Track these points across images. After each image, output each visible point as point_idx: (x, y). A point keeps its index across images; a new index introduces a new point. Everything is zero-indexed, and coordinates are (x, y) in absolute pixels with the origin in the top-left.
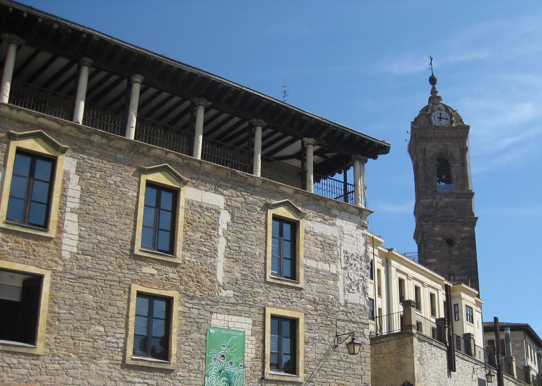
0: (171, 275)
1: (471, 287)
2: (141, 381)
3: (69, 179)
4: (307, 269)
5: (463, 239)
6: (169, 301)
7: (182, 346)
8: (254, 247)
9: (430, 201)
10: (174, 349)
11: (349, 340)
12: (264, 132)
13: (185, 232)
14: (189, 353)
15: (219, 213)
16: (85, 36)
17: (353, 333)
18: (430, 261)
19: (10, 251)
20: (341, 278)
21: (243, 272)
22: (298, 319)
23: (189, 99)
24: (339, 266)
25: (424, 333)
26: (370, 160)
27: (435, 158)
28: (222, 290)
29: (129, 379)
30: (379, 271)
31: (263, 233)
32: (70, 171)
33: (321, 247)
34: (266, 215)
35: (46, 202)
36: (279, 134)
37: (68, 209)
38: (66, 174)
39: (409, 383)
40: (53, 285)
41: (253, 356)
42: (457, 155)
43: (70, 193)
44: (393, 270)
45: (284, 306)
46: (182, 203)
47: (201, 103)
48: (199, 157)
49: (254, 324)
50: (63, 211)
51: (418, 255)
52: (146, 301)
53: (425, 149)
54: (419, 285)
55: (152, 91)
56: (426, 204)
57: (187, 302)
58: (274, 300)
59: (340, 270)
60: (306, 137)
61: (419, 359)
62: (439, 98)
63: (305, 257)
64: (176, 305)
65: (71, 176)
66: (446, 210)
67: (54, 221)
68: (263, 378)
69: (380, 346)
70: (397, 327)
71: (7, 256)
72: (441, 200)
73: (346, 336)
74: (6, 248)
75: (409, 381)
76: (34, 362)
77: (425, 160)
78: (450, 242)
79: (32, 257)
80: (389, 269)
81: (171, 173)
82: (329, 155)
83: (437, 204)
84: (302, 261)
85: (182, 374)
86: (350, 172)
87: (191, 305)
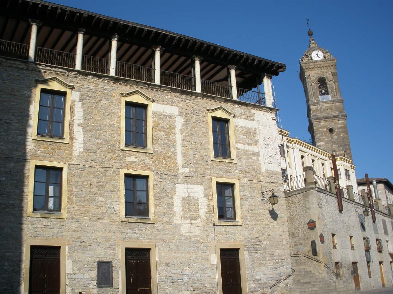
4: (238, 150)
5: (339, 128)
8: (201, 139)
9: (316, 107)
12: (202, 65)
13: (153, 132)
14: (162, 211)
16: (78, 14)
17: (272, 190)
20: (261, 154)
23: (151, 48)
27: (317, 80)
32: (75, 100)
36: (212, 65)
40: (70, 173)
41: (206, 210)
43: (76, 113)
45: (224, 176)
49: (205, 189)
51: (312, 141)
53: (310, 75)
55: (126, 46)
56: (315, 109)
60: (229, 65)
64: (151, 181)
65: (76, 103)
66: (327, 111)
69: (292, 198)
72: (323, 105)
73: (268, 193)
74: (38, 153)
78: (331, 130)
81: (142, 95)
83: (321, 108)
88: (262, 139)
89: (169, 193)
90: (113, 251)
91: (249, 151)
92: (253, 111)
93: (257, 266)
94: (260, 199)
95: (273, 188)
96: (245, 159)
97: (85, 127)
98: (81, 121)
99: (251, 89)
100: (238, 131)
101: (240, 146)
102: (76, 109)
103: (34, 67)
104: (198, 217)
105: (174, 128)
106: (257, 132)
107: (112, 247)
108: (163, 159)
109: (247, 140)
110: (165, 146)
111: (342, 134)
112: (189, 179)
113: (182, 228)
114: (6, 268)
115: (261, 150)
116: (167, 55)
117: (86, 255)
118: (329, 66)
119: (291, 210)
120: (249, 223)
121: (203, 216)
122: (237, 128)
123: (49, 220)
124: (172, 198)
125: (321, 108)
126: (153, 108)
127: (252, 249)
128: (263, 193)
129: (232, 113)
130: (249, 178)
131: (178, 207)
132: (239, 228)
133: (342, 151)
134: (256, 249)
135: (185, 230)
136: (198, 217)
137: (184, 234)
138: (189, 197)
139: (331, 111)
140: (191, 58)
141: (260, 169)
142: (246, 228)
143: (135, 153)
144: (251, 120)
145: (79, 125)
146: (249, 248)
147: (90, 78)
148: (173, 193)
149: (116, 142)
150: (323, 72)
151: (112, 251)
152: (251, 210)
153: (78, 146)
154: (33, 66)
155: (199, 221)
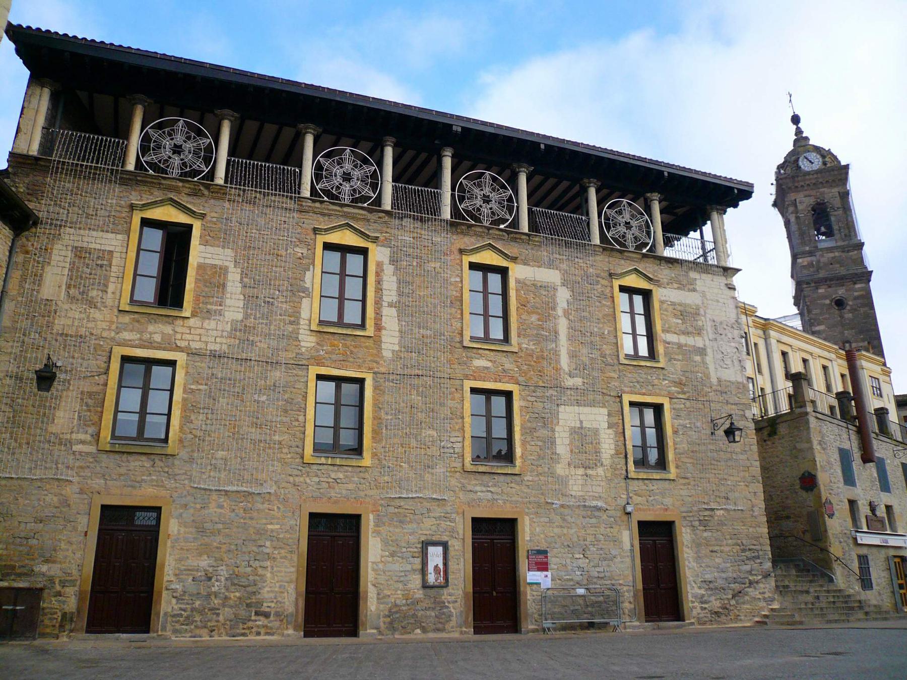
0: (508, 366)
1: (874, 353)
2: (484, 489)
3: (383, 270)
4: (667, 345)
5: (856, 298)
6: (508, 395)
7: (528, 446)
9: (809, 259)
10: (518, 451)
11: (727, 425)
13: (519, 315)
15: (555, 289)
18: (817, 328)
19: (327, 356)
20: (709, 351)
21: (590, 355)
22: (662, 404)
24: (706, 338)
25: (820, 410)
26: (730, 210)
28: (568, 378)
29: (470, 487)
30: (756, 344)
31: (610, 308)
33: (682, 317)
34: (612, 287)
35: (361, 298)
37: (385, 304)
38: (379, 265)
39: (809, 473)
40: (376, 388)
41: (613, 452)
42: (837, 202)
43: (385, 285)
44: (773, 342)
45: (644, 391)
46: (512, 283)
47: (521, 170)
48: (526, 230)
49: (609, 415)
50: (379, 306)
52: (482, 398)
53: (795, 200)
54: (807, 356)
57: (529, 395)
58: (631, 384)
59: (707, 342)
61: (820, 443)
62: (807, 139)
63: (663, 331)
65: (385, 267)
66: (831, 266)
67: (371, 319)
68: (627, 478)
70: (785, 408)
71: (323, 361)
72: (822, 256)
73: (722, 421)
74: (322, 353)
75: (809, 470)
76: (362, 475)
77: (797, 213)
79: (351, 359)
80: (768, 342)
82: (680, 211)
83: (818, 262)
84: (660, 336)
85: (530, 478)
86: (707, 228)
87: (533, 399)
88: (709, 324)
89: (546, 421)
90: (451, 524)
91: (686, 345)
92: (693, 275)
93: (706, 556)
94: (709, 432)
95: (732, 412)
96: (680, 360)
97: (400, 307)
98: (395, 299)
99: (686, 235)
100: (666, 310)
101: (671, 338)
102: (385, 278)
103: (310, 207)
104: (598, 463)
105: (554, 309)
106: (702, 312)
107: (448, 515)
108: (535, 362)
109: (683, 327)
110: (539, 339)
111: (862, 310)
112: (582, 398)
113: (571, 482)
114: (267, 551)
115: (707, 342)
116: (538, 179)
117: (405, 531)
118: (833, 181)
119: (766, 453)
120: (689, 475)
121: (607, 461)
122: (665, 306)
123: (341, 469)
124: (553, 431)
125: (818, 262)
126: (517, 272)
127: (697, 523)
128: (715, 422)
129: (656, 278)
130: (688, 395)
131: (562, 447)
132: (673, 484)
133: (864, 341)
134: (704, 523)
135: (575, 488)
136: (598, 463)
137: (573, 493)
138: (582, 428)
139: (838, 266)
140: (580, 184)
141: (709, 378)
142: (684, 485)
143: (487, 352)
144: (689, 290)
145: (390, 305)
146: (691, 521)
147: (406, 222)
148: (555, 421)
149: (455, 334)
150: (823, 193)
151: (448, 523)
152: (692, 452)
153: (390, 342)
154: (310, 204)
155: (600, 471)
